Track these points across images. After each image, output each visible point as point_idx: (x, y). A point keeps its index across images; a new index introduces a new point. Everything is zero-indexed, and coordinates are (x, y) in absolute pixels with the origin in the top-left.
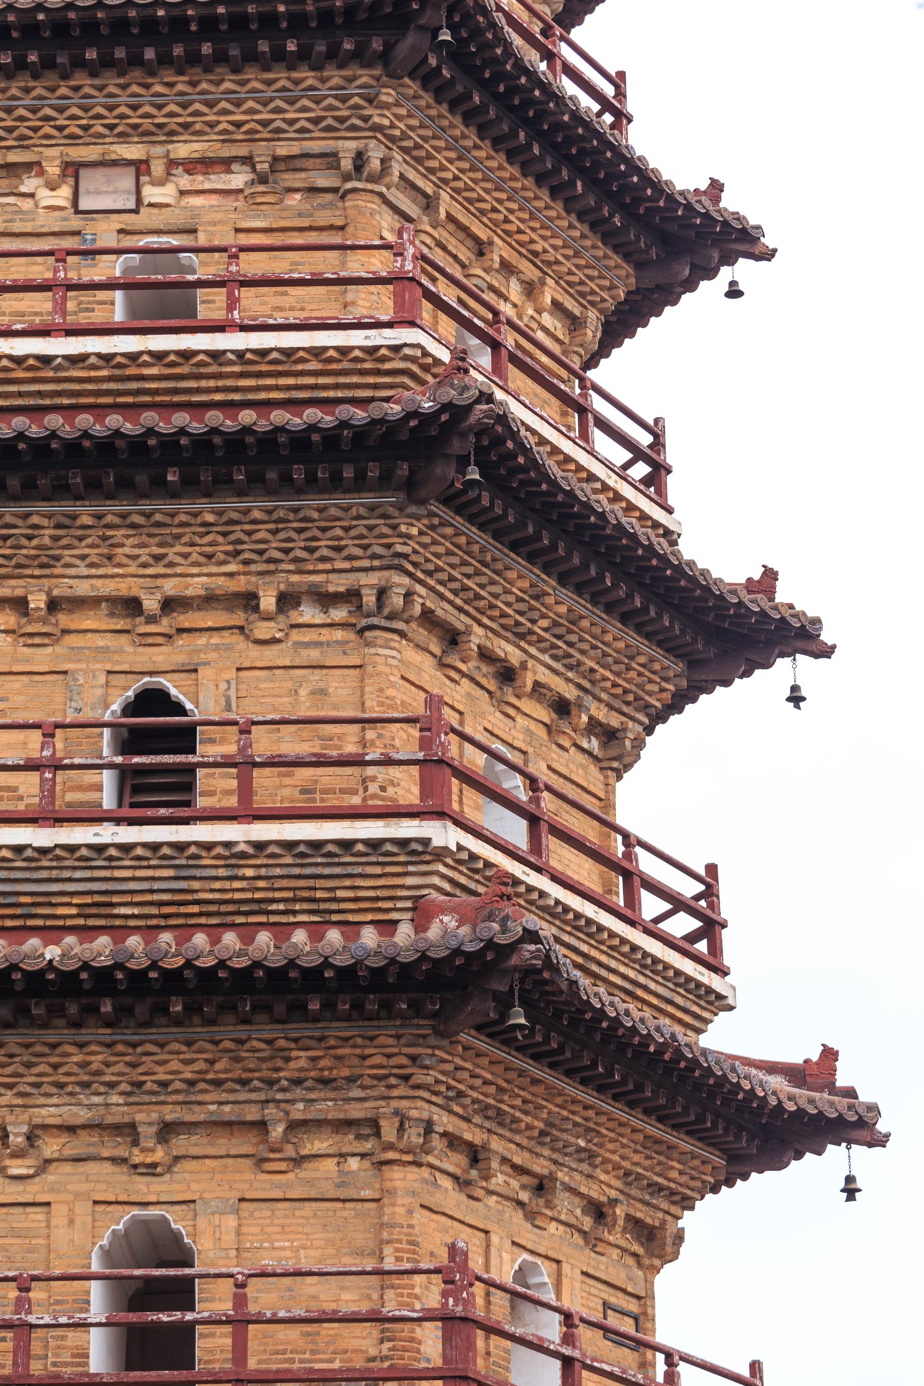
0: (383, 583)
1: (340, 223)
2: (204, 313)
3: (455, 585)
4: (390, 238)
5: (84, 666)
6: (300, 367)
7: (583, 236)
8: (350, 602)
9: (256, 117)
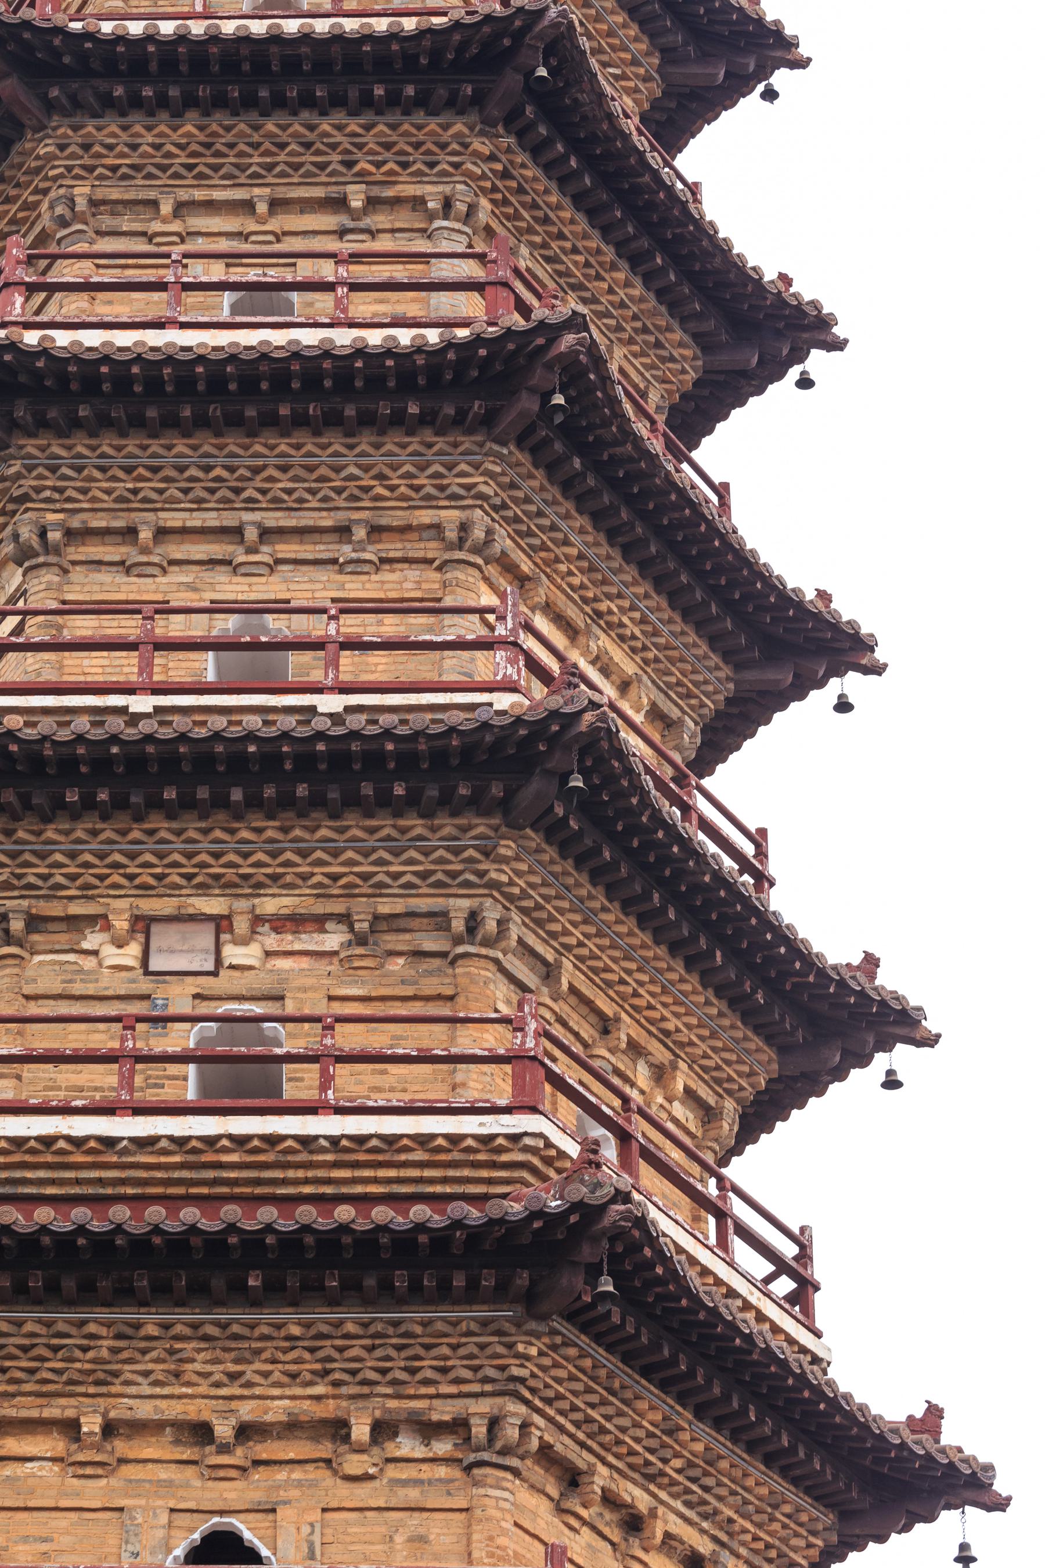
0: (496, 1411)
1: (449, 992)
2: (290, 1092)
3: (578, 1416)
4: (505, 1010)
5: (143, 1502)
6: (403, 1157)
7: (721, 1014)
8: (456, 1433)
9: (356, 869)
